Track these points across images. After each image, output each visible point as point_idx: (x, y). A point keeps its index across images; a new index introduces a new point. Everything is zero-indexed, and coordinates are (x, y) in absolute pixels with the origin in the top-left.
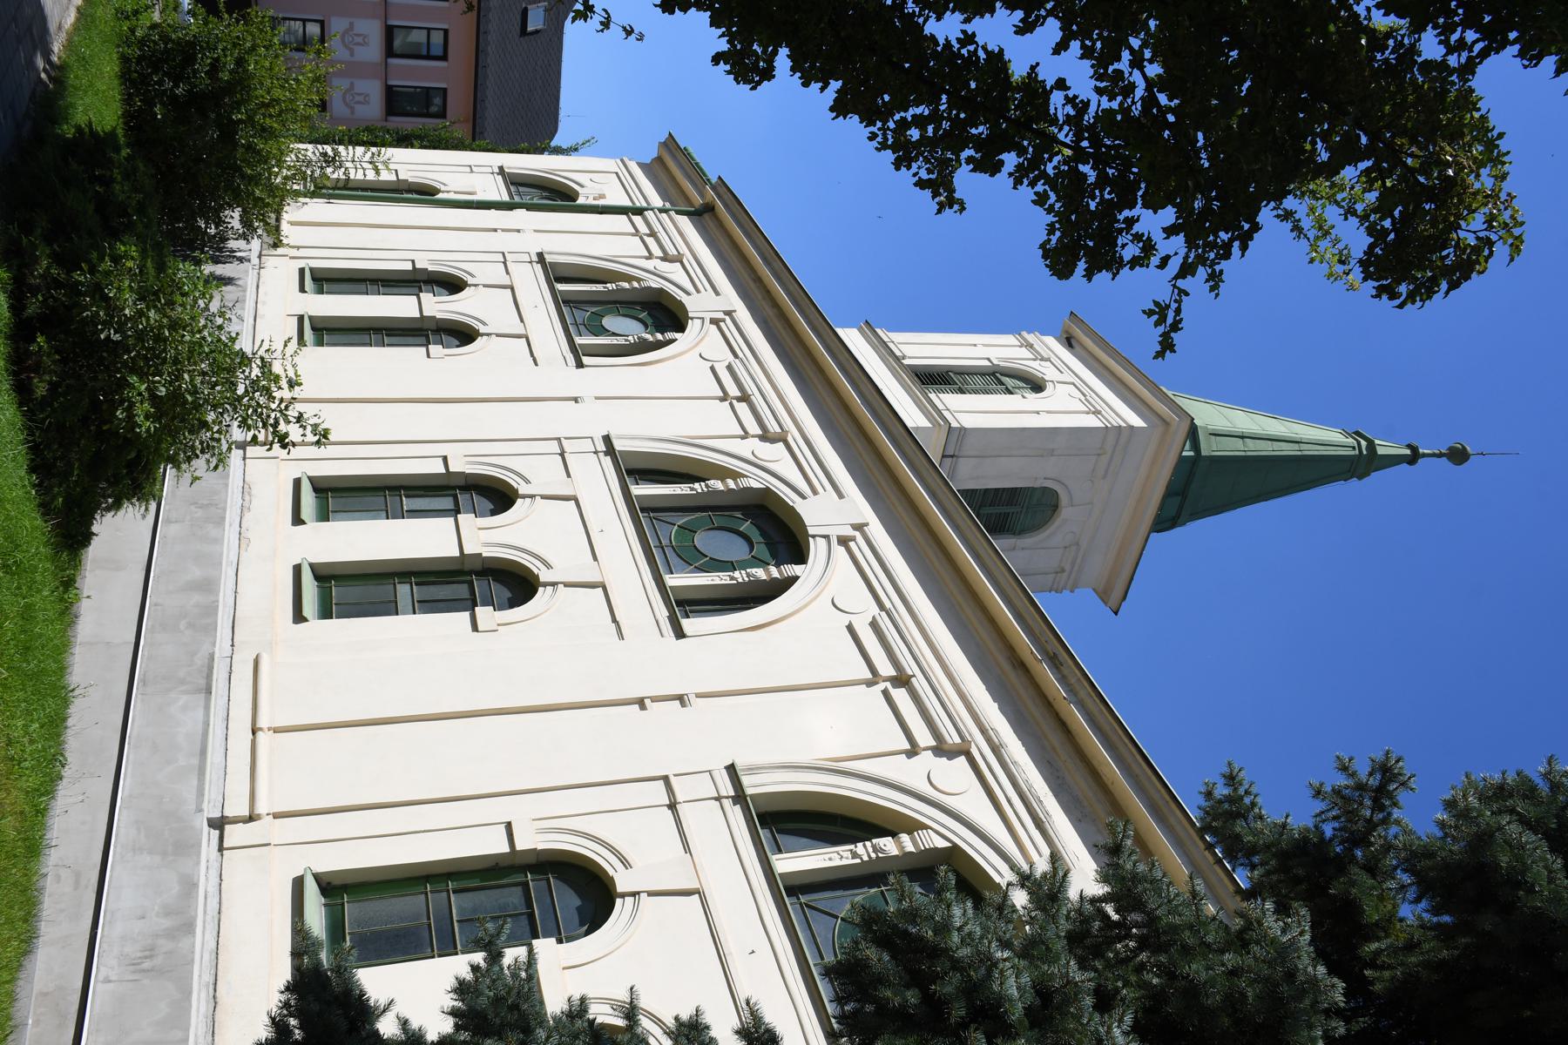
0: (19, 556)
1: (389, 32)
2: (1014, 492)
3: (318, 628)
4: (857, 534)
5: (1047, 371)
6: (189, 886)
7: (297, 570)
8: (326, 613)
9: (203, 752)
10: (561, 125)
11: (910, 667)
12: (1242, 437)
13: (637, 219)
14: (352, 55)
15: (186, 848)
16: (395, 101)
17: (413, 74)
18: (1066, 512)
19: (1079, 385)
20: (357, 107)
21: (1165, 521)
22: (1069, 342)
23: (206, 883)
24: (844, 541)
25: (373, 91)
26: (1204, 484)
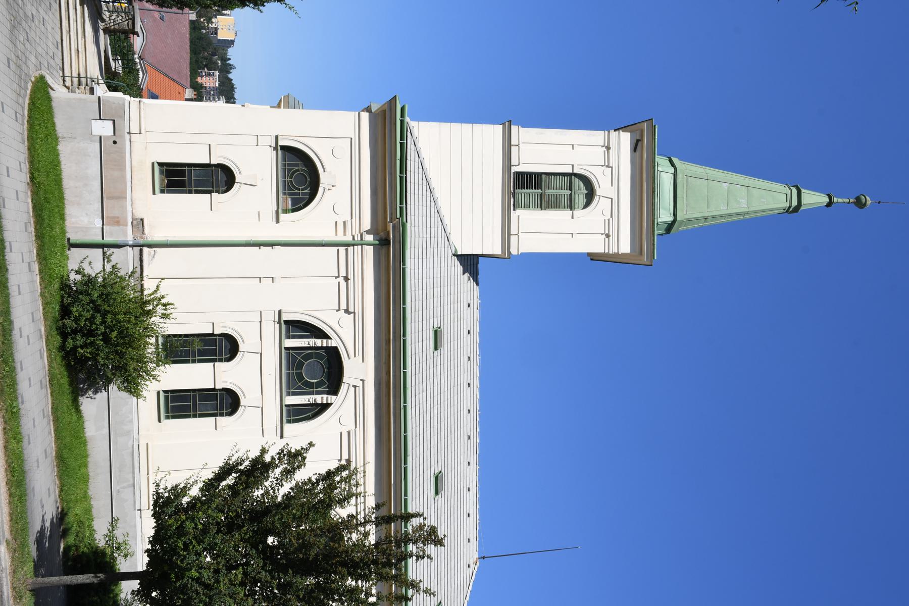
4: (360, 384)
5: (603, 187)
11: (351, 276)
12: (706, 219)
13: (342, 250)
22: (636, 146)
24: (355, 387)
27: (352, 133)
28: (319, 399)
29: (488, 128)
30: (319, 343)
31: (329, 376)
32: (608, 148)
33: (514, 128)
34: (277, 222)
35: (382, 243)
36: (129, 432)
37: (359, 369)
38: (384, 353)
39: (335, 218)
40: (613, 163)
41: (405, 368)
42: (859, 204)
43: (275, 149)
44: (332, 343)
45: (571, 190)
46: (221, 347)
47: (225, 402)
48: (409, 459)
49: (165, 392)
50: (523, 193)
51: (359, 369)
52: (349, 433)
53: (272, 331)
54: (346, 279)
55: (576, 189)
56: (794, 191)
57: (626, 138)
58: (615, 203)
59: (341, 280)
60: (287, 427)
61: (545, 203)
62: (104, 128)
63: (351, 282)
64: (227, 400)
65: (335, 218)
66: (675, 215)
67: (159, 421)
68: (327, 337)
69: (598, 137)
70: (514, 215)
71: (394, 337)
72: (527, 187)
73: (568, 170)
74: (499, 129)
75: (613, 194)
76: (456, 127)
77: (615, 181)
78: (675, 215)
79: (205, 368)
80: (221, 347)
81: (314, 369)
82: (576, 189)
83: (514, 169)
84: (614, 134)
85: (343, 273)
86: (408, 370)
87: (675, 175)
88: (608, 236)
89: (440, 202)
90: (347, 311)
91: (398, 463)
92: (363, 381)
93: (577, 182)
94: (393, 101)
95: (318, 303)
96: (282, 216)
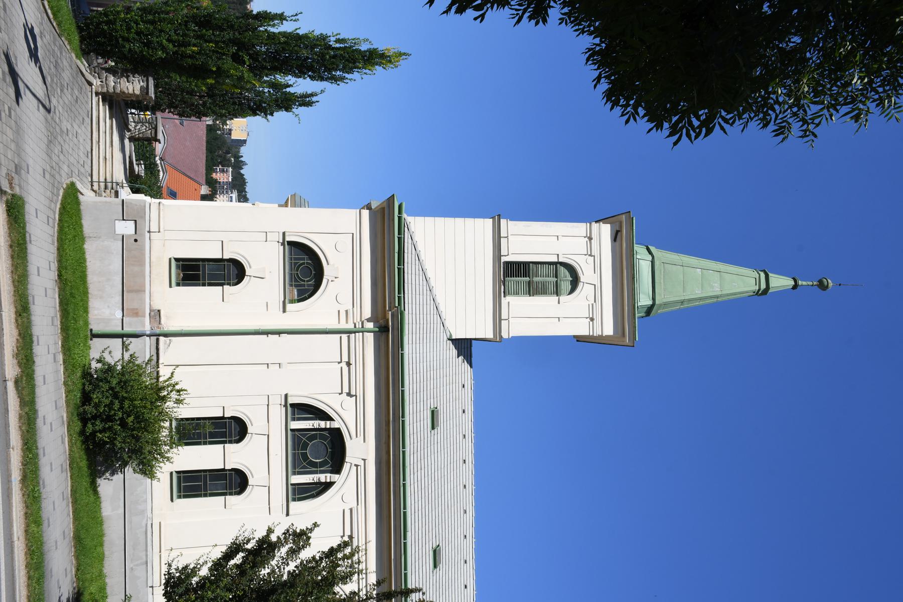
5: (586, 274)
7: (170, 259)
11: (352, 361)
12: (682, 302)
13: (345, 337)
19: (598, 289)
22: (616, 236)
24: (357, 466)
27: (353, 229)
30: (323, 424)
32: (590, 239)
33: (503, 221)
34: (284, 311)
35: (382, 330)
37: (361, 449)
40: (595, 252)
41: (404, 480)
42: (822, 286)
43: (283, 244)
44: (335, 425)
45: (556, 277)
46: (231, 429)
47: (234, 482)
48: (409, 534)
51: (361, 449)
52: (351, 510)
53: (278, 414)
54: (348, 364)
55: (561, 277)
56: (763, 275)
57: (606, 230)
59: (344, 365)
60: (293, 505)
61: (533, 290)
63: (353, 367)
64: (233, 270)
66: (654, 299)
68: (330, 419)
69: (580, 228)
70: (504, 301)
71: (394, 417)
72: (516, 275)
74: (489, 222)
77: (598, 268)
78: (654, 299)
80: (231, 429)
81: (317, 449)
82: (561, 277)
83: (504, 259)
84: (595, 226)
85: (345, 359)
87: (648, 249)
88: (592, 319)
89: (435, 291)
90: (349, 394)
91: (396, 342)
92: (364, 460)
93: (562, 271)
94: (391, 199)
96: (289, 307)
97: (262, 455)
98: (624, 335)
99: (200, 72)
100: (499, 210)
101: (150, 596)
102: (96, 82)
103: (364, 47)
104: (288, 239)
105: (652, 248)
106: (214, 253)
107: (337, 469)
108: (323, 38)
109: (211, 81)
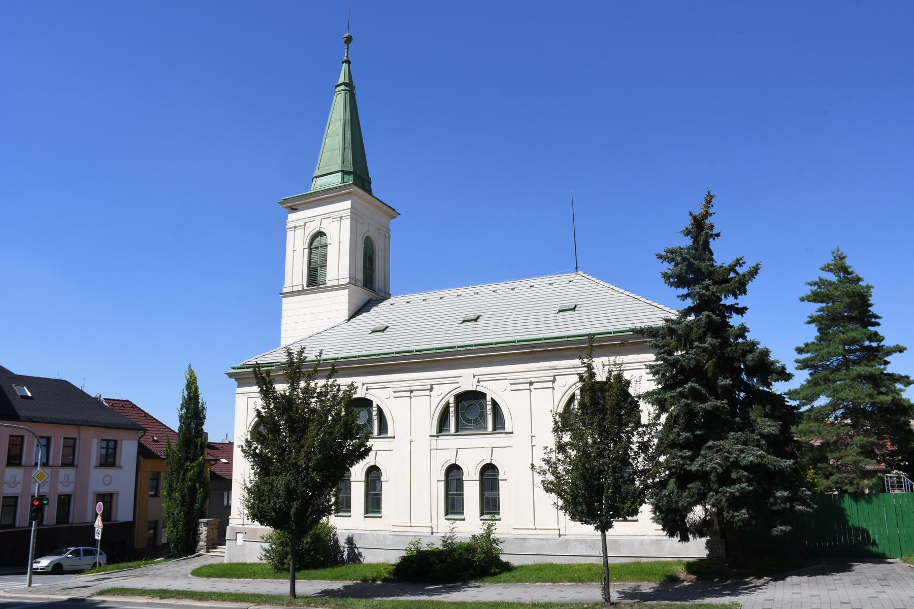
0: (823, 483)
1: (64, 465)
2: (365, 255)
3: (465, 516)
4: (477, 377)
5: (313, 228)
6: (576, 540)
8: (349, 511)
9: (164, 594)
10: (63, 378)
11: (529, 380)
12: (344, 148)
14: (19, 483)
15: (567, 541)
16: (68, 463)
17: (57, 455)
18: (370, 234)
19: (325, 217)
20: (18, 480)
21: (369, 192)
22: (294, 209)
23: (574, 538)
25: (64, 472)
26: (359, 175)
27: (245, 397)
28: (489, 407)
29: (284, 307)
30: (452, 409)
31: (365, 406)
32: (295, 227)
33: (285, 291)
36: (384, 536)
37: (466, 379)
38: (349, 371)
39: (392, 397)
41: (492, 344)
42: (349, 40)
43: (437, 436)
44: (452, 400)
46: (453, 473)
48: (411, 348)
49: (481, 515)
50: (320, 279)
51: (466, 379)
53: (445, 441)
54: (531, 383)
56: (338, 89)
57: (292, 217)
58: (325, 217)
59: (532, 387)
60: (507, 430)
62: (240, 536)
63: (533, 380)
64: (454, 473)
65: (392, 397)
66: (338, 172)
67: (464, 520)
69: (290, 235)
70: (329, 284)
73: (306, 251)
74: (284, 300)
75: (318, 219)
76: (283, 328)
78: (338, 172)
79: (354, 486)
80: (453, 473)
81: (469, 412)
83: (305, 288)
84: (289, 225)
85: (527, 386)
86: (493, 341)
88: (341, 218)
89: (311, 333)
92: (474, 376)
93: (315, 244)
95: (426, 410)
96: (507, 430)
97: (471, 451)
98: (350, 193)
99: (193, 490)
100: (279, 294)
101: (566, 537)
102: (201, 552)
103: (186, 393)
104: (435, 433)
105: (316, 173)
106: (442, 485)
107: (483, 395)
108: (181, 417)
109: (197, 485)
